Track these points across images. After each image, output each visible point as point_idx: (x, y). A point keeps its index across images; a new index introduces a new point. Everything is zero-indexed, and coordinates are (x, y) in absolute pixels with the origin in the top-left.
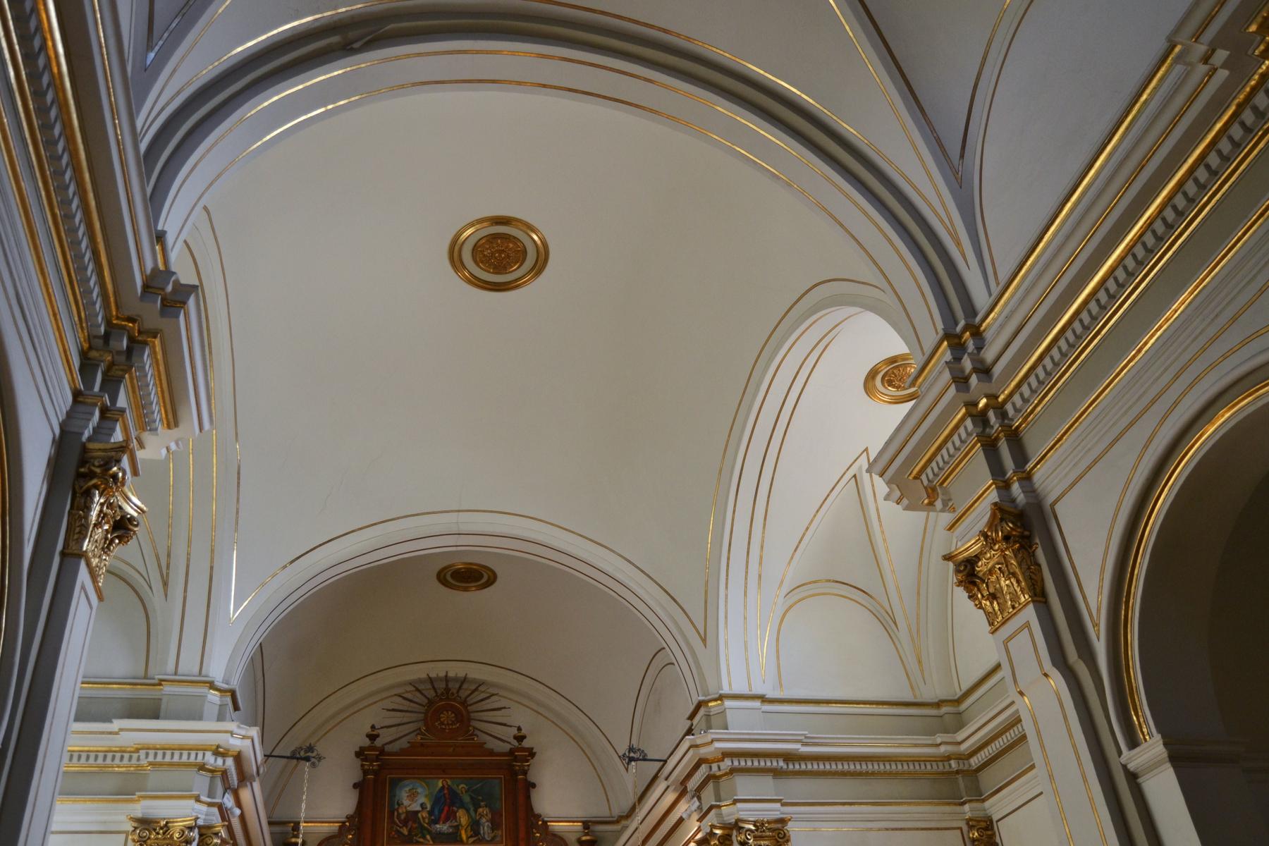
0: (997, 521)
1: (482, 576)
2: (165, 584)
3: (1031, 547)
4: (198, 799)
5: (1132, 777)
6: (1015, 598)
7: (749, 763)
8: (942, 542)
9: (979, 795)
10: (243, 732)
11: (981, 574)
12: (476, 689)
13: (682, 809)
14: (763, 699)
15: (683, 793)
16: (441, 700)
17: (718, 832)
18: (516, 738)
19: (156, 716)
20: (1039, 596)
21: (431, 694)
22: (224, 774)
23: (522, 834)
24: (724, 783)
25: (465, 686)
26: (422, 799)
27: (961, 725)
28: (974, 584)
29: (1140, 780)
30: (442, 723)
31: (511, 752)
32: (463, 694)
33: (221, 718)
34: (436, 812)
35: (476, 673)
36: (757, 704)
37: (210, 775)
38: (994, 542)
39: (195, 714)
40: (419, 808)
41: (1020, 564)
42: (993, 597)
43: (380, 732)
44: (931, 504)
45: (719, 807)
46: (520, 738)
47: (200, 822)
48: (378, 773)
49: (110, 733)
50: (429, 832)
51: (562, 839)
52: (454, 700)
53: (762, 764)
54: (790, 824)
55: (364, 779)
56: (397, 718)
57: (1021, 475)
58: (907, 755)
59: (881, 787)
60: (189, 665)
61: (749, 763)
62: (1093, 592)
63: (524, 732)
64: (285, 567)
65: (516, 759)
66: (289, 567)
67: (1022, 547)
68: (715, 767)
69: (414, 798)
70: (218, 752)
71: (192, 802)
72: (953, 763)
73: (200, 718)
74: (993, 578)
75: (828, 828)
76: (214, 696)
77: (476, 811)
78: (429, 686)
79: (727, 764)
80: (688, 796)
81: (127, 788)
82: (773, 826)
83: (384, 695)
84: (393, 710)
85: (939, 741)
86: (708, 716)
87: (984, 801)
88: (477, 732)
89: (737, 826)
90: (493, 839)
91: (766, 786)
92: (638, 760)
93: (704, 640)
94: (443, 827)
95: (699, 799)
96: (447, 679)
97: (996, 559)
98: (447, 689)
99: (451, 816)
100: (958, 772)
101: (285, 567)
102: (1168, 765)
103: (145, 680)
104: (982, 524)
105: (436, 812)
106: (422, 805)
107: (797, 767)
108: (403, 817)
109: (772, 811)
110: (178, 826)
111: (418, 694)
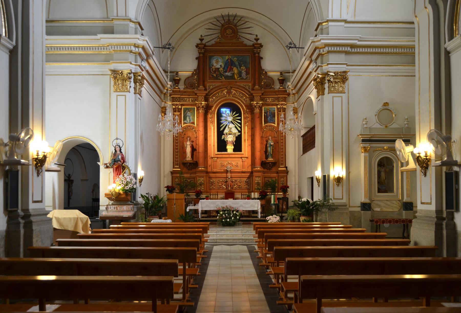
4: (131, 63)
5: (448, 53)
10: (143, 38)
12: (240, 20)
14: (346, 21)
15: (311, 61)
16: (227, 24)
18: (255, 39)
19: (113, 33)
22: (140, 54)
24: (325, 57)
25: (236, 18)
26: (220, 63)
29: (450, 55)
30: (227, 34)
31: (253, 45)
33: (136, 33)
34: (226, 68)
35: (240, 13)
36: (343, 24)
39: (126, 32)
40: (219, 67)
45: (322, 66)
46: (257, 40)
47: (133, 71)
48: (205, 53)
49: (98, 39)
51: (272, 79)
52: (231, 24)
54: (349, 74)
56: (211, 32)
59: (375, 59)
60: (122, 13)
61: (333, 49)
63: (258, 37)
69: (218, 63)
70: (136, 46)
71: (129, 64)
73: (128, 33)
76: (132, 25)
77: (240, 68)
78: (222, 19)
80: (313, 62)
81: (107, 59)
83: (203, 24)
84: (249, 28)
86: (322, 29)
88: (240, 37)
89: (327, 74)
90: (247, 78)
91: (342, 58)
92: (293, 48)
94: (228, 74)
95: (316, 63)
96: (229, 16)
98: (229, 20)
99: (231, 70)
103: (107, 18)
105: (226, 68)
106: (221, 66)
108: (214, 70)
109: (343, 68)
110: (125, 72)
111: (218, 22)
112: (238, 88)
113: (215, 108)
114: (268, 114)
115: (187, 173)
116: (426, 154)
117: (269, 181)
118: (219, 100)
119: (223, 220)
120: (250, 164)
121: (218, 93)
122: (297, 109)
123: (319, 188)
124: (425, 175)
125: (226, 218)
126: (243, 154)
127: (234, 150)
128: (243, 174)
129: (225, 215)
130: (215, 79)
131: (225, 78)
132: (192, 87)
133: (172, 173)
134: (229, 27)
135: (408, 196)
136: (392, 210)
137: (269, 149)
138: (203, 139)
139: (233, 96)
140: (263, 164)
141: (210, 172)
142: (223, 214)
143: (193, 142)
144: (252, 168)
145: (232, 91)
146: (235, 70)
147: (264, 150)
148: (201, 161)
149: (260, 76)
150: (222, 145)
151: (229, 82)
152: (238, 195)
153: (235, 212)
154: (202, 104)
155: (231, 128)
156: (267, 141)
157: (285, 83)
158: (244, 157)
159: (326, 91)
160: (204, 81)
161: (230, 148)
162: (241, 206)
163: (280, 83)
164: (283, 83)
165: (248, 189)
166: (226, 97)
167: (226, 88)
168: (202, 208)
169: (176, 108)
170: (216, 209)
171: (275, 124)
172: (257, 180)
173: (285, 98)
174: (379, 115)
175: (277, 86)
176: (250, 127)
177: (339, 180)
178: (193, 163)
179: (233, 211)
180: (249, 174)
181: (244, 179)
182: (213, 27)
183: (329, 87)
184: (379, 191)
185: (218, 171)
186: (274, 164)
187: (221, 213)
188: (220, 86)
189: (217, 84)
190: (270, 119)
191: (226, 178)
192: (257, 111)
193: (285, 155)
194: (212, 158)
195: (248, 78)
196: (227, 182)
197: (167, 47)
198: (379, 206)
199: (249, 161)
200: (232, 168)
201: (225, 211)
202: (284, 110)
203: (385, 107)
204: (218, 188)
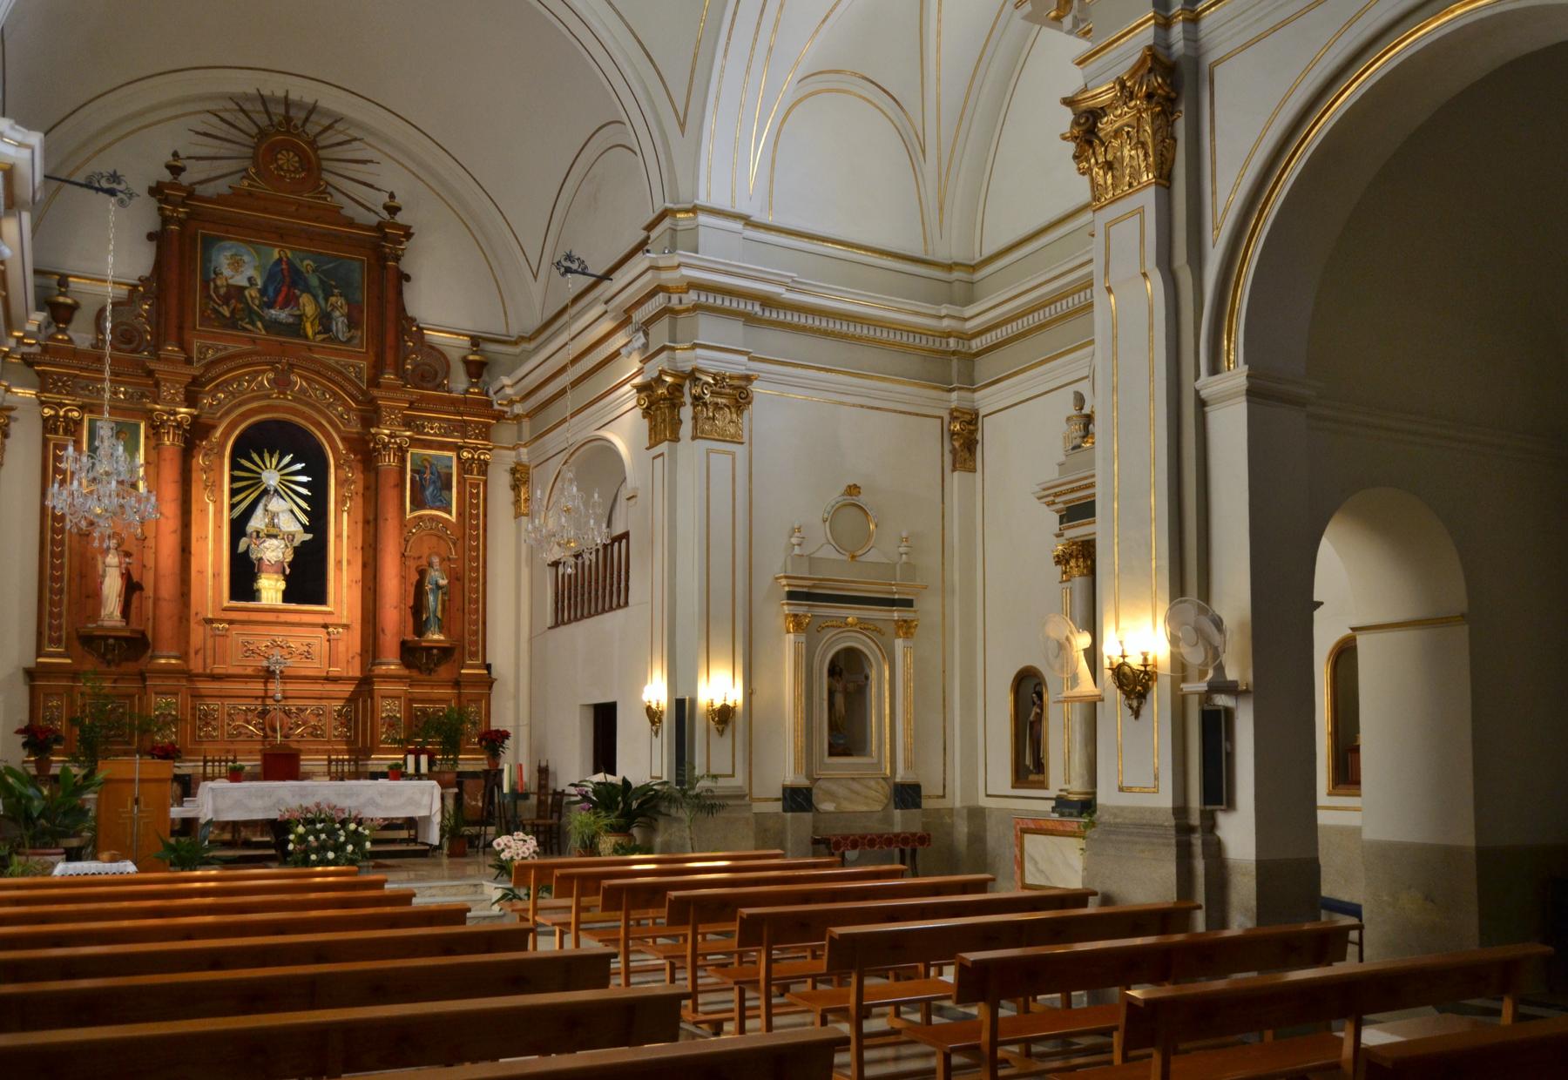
0: (1143, 71)
3: (1172, 114)
5: (1201, 404)
6: (1136, 174)
7: (719, 302)
8: (1072, 82)
9: (970, 384)
10: (19, 137)
11: (1101, 134)
12: (330, 127)
13: (619, 340)
14: (747, 220)
17: (669, 379)
18: (386, 207)
20: (1164, 179)
21: (263, 120)
23: (390, 338)
24: (682, 320)
25: (314, 117)
26: (250, 272)
27: (969, 300)
28: (1090, 143)
30: (280, 168)
31: (380, 227)
32: (312, 129)
34: (271, 291)
35: (332, 101)
36: (738, 226)
38: (1132, 96)
40: (245, 283)
41: (1154, 133)
42: (1109, 166)
43: (186, 163)
44: (1058, 19)
45: (673, 349)
46: (393, 210)
48: (185, 227)
50: (261, 319)
51: (442, 353)
52: (298, 136)
53: (735, 305)
57: (1190, 16)
58: (894, 322)
62: (1227, 191)
63: (398, 201)
65: (385, 237)
67: (1163, 112)
68: (675, 298)
69: (239, 268)
72: (952, 341)
74: (1116, 143)
75: (796, 395)
77: (326, 300)
78: (260, 107)
79: (691, 297)
80: (630, 328)
82: (736, 383)
83: (178, 110)
85: (943, 312)
87: (974, 391)
88: (330, 189)
89: (693, 376)
90: (349, 340)
91: (734, 333)
92: (576, 272)
93: (682, 125)
94: (281, 315)
95: (646, 334)
97: (1126, 119)
98: (288, 119)
99: (290, 301)
100: (954, 353)
102: (1244, 398)
104: (1123, 69)
105: (271, 291)
106: (250, 279)
107: (774, 315)
108: (222, 291)
109: (736, 365)
111: (241, 115)
112: (318, 373)
113: (226, 435)
114: (427, 476)
116: (1145, 659)
118: (240, 405)
120: (358, 650)
121: (238, 379)
122: (527, 468)
123: (657, 742)
124: (1137, 714)
126: (330, 613)
127: (288, 596)
128: (329, 687)
129: (317, 838)
130: (225, 326)
131: (266, 328)
132: (130, 342)
133: (31, 674)
134: (287, 144)
135: (909, 765)
136: (865, 809)
138: (178, 550)
139: (295, 399)
140: (409, 653)
141: (198, 675)
142: (308, 833)
143: (128, 554)
145: (294, 378)
146: (308, 306)
148: (167, 628)
149: (399, 340)
150: (244, 576)
151: (281, 343)
152: (307, 763)
154: (176, 413)
155: (274, 515)
156: (422, 573)
157: (485, 377)
158: (336, 626)
159: (686, 429)
160: (181, 328)
161: (271, 588)
162: (372, 802)
163: (470, 375)
164: (479, 376)
166: (268, 397)
167: (272, 364)
169: (56, 416)
170: (274, 815)
171: (450, 513)
172: (389, 704)
173: (488, 426)
174: (833, 518)
175: (459, 382)
176: (360, 518)
177: (724, 715)
178: (126, 639)
179: (344, 823)
182: (221, 129)
183: (695, 418)
184: (834, 751)
185: (231, 671)
186: (446, 653)
188: (250, 354)
189: (233, 348)
190: (434, 497)
191: (264, 698)
192: (389, 461)
193: (484, 623)
194: (210, 621)
195: (356, 341)
197: (105, 185)
198: (832, 796)
199: (351, 642)
201: (312, 822)
202: (484, 467)
203: (849, 499)
204: (230, 735)
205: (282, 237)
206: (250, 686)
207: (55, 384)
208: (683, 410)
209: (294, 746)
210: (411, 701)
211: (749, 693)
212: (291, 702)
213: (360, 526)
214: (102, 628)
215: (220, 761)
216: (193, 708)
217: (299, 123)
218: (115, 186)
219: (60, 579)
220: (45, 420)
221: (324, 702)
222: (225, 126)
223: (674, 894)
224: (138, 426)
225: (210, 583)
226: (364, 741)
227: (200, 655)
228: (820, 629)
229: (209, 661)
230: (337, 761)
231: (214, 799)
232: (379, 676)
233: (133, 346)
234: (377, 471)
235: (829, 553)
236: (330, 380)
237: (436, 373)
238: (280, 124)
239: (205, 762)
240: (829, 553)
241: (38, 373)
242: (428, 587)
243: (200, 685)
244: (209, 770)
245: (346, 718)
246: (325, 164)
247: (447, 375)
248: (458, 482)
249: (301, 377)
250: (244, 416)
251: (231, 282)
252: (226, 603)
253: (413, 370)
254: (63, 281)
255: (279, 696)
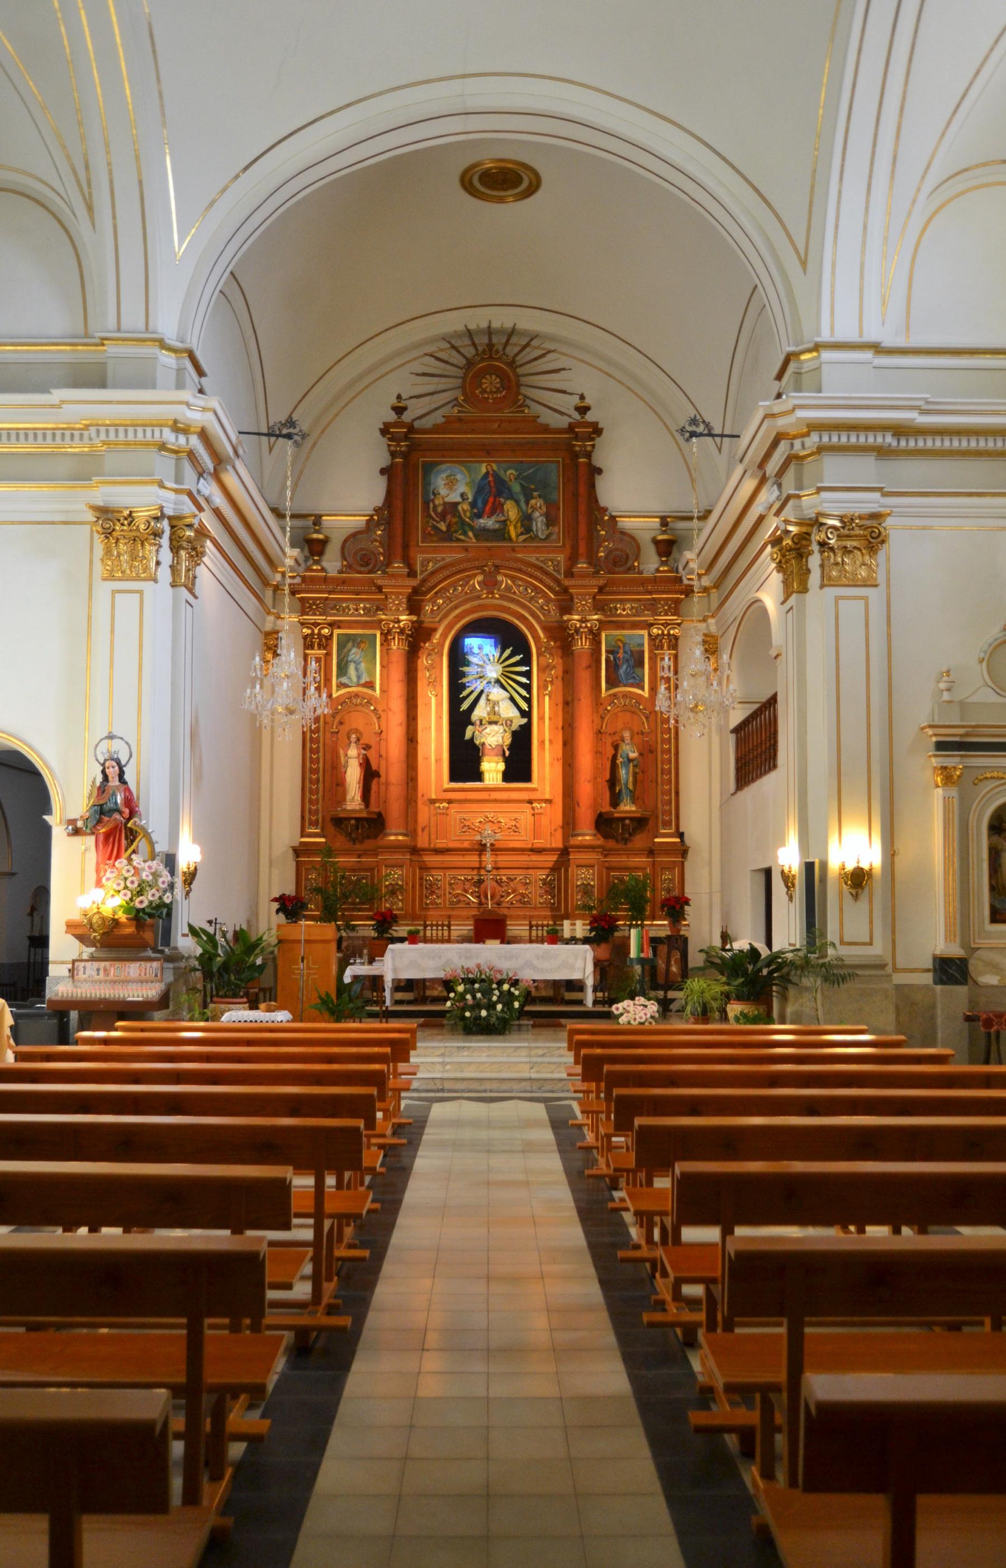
1: (519, 181)
2: (90, 208)
4: (161, 485)
10: (202, 403)
12: (527, 345)
14: (877, 348)
15: (763, 481)
16: (483, 360)
19: (103, 385)
21: (470, 352)
22: (191, 455)
24: (809, 467)
25: (514, 340)
30: (484, 391)
31: (571, 428)
32: (511, 351)
33: (180, 385)
34: (480, 504)
35: (527, 321)
36: (868, 355)
37: (174, 456)
40: (459, 499)
45: (799, 497)
46: (583, 410)
47: (169, 512)
48: (410, 455)
50: (472, 529)
52: (499, 359)
53: (862, 439)
55: (392, 464)
60: (133, 319)
63: (588, 401)
64: (237, 177)
66: (243, 176)
68: (797, 443)
69: (453, 486)
70: (178, 428)
71: (155, 489)
73: (153, 386)
76: (168, 359)
77: (527, 503)
78: (468, 342)
81: (84, 470)
82: (868, 523)
84: (424, 374)
88: (528, 402)
89: (816, 523)
90: (548, 536)
91: (864, 469)
92: (701, 435)
93: (804, 263)
94: (489, 522)
95: (780, 486)
96: (490, 331)
98: (490, 345)
99: (497, 509)
101: (237, 177)
105: (480, 504)
106: (462, 495)
108: (440, 509)
110: (142, 515)
111: (454, 353)
112: (520, 571)
113: (444, 636)
114: (621, 655)
115: (347, 853)
117: (621, 880)
118: (456, 607)
119: (468, 1014)
120: (561, 823)
121: (454, 585)
123: (792, 906)
125: (477, 1006)
126: (534, 790)
127: (507, 776)
128: (535, 858)
129: (474, 997)
131: (476, 536)
137: (622, 772)
140: (604, 823)
141: (424, 850)
142: (466, 991)
143: (367, 747)
144: (566, 837)
145: (499, 578)
147: (608, 777)
149: (592, 531)
150: (465, 761)
151: (489, 548)
152: (516, 928)
153: (506, 987)
154: (399, 621)
155: (496, 703)
156: (616, 747)
157: (675, 554)
159: (814, 578)
160: (406, 547)
161: (492, 769)
162: (529, 964)
163: (660, 554)
165: (553, 908)
166: (479, 597)
167: (480, 568)
168: (395, 970)
169: (313, 634)
170: (441, 975)
172: (583, 875)
173: (677, 602)
175: (651, 563)
176: (560, 700)
179: (500, 983)
180: (554, 858)
181: (540, 872)
183: (822, 566)
186: (640, 823)
187: (461, 988)
188: (459, 562)
189: (449, 557)
190: (627, 674)
191: (479, 868)
192: (582, 645)
193: (677, 793)
194: (433, 802)
195: (554, 537)
196: (480, 882)
197: (285, 431)
198: (994, 968)
199: (554, 815)
200: (498, 836)
201: (473, 982)
202: (674, 643)
204: (452, 903)
205: (488, 453)
206: (468, 858)
207: (310, 607)
208: (811, 559)
209: (506, 912)
210: (610, 869)
211: (890, 853)
212: (502, 872)
213: (560, 707)
214: (345, 810)
215: (437, 925)
216: (421, 879)
217: (500, 348)
218: (291, 430)
219: (317, 771)
220: (305, 638)
221: (530, 872)
222: (442, 365)
223: (606, 1068)
224: (375, 635)
225: (433, 768)
226: (566, 907)
227: (426, 831)
228: (977, 782)
229: (432, 837)
230: (537, 926)
231: (393, 958)
232: (573, 847)
233: (370, 567)
234: (572, 653)
235: (987, 696)
236: (531, 576)
237: (627, 556)
238: (484, 351)
239: (425, 926)
240: (987, 696)
241: (302, 600)
242: (619, 760)
243: (426, 858)
244: (534, 933)
245: (550, 887)
246: (523, 380)
247: (637, 558)
248: (650, 658)
249: (506, 575)
250: (459, 617)
251: (446, 500)
252: (447, 784)
253: (606, 557)
254: (318, 520)
255: (489, 867)
